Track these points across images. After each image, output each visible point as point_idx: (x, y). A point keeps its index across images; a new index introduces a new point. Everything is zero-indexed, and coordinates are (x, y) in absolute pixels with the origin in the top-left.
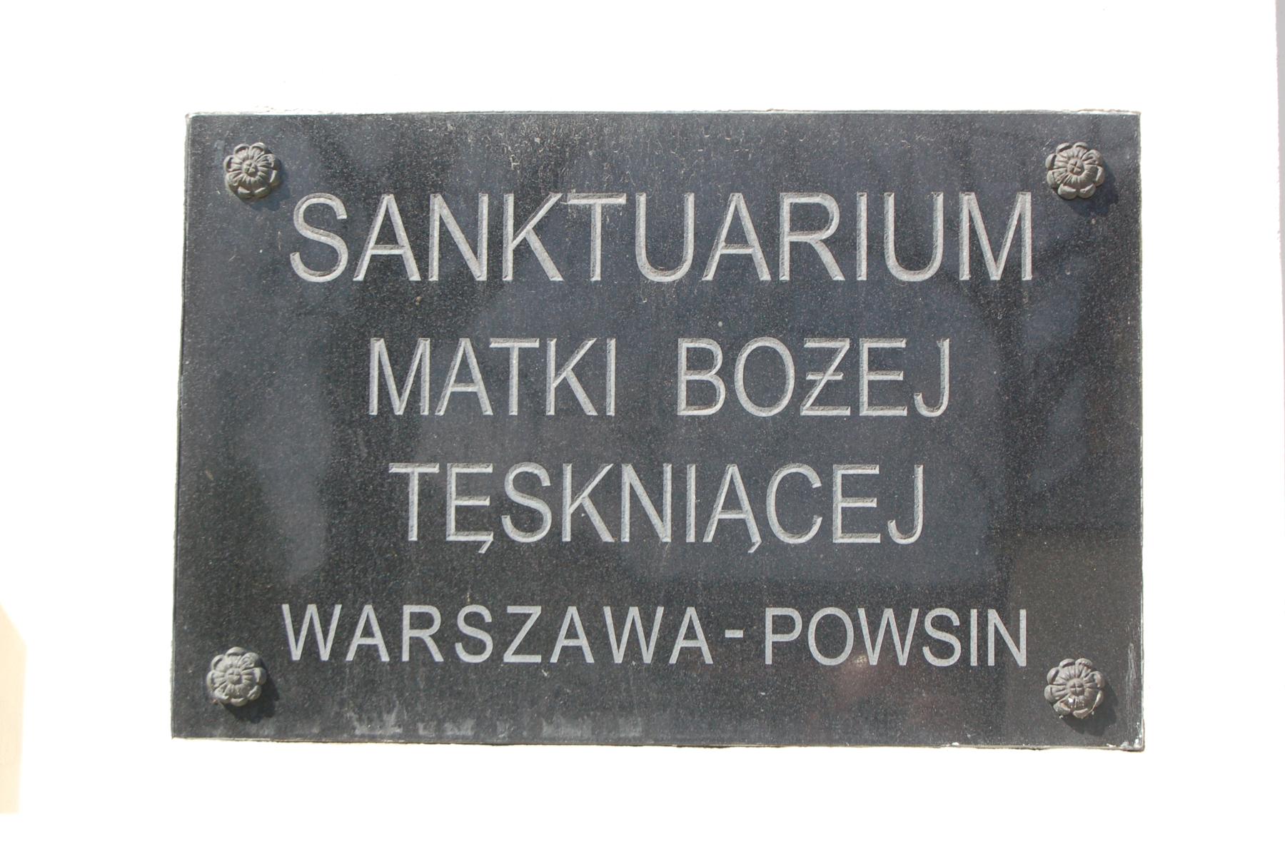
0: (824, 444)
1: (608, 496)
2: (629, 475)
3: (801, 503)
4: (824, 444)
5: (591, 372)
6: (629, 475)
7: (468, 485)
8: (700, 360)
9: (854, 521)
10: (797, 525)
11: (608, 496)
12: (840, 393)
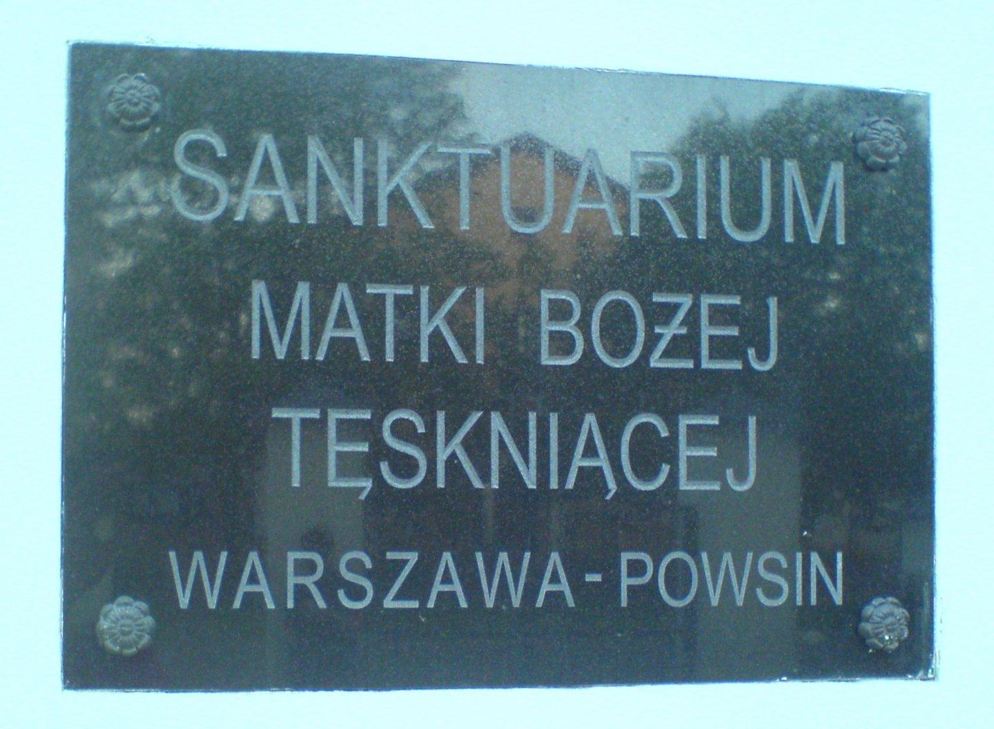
0: (670, 394)
1: (478, 443)
2: (497, 423)
3: (651, 452)
4: (670, 394)
5: (461, 323)
6: (497, 423)
7: (348, 430)
8: (560, 311)
9: (699, 469)
10: (645, 469)
11: (478, 443)
12: (685, 345)
